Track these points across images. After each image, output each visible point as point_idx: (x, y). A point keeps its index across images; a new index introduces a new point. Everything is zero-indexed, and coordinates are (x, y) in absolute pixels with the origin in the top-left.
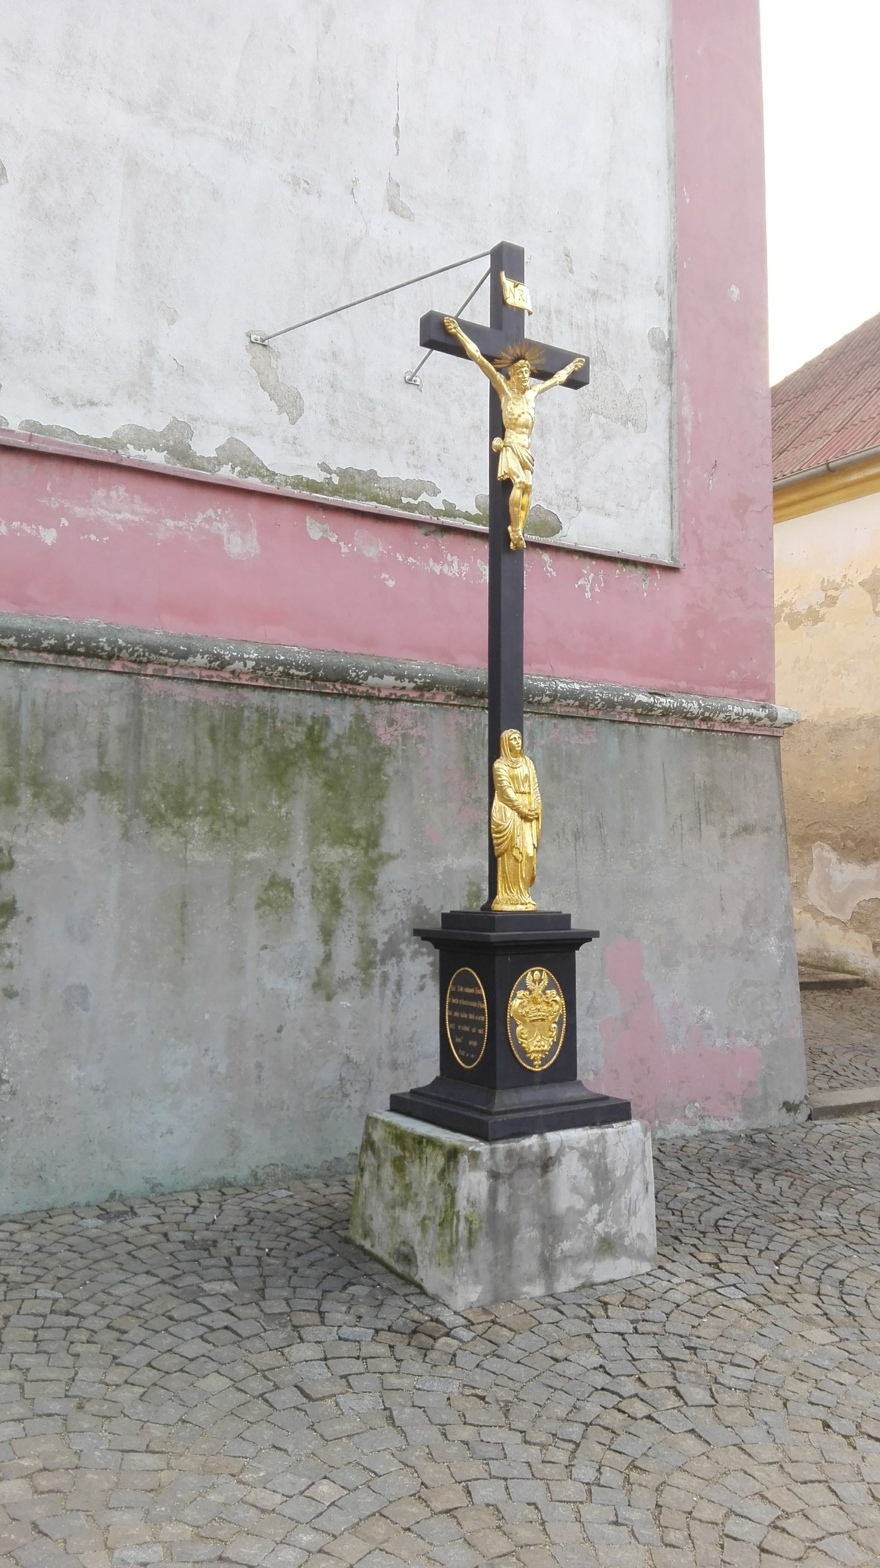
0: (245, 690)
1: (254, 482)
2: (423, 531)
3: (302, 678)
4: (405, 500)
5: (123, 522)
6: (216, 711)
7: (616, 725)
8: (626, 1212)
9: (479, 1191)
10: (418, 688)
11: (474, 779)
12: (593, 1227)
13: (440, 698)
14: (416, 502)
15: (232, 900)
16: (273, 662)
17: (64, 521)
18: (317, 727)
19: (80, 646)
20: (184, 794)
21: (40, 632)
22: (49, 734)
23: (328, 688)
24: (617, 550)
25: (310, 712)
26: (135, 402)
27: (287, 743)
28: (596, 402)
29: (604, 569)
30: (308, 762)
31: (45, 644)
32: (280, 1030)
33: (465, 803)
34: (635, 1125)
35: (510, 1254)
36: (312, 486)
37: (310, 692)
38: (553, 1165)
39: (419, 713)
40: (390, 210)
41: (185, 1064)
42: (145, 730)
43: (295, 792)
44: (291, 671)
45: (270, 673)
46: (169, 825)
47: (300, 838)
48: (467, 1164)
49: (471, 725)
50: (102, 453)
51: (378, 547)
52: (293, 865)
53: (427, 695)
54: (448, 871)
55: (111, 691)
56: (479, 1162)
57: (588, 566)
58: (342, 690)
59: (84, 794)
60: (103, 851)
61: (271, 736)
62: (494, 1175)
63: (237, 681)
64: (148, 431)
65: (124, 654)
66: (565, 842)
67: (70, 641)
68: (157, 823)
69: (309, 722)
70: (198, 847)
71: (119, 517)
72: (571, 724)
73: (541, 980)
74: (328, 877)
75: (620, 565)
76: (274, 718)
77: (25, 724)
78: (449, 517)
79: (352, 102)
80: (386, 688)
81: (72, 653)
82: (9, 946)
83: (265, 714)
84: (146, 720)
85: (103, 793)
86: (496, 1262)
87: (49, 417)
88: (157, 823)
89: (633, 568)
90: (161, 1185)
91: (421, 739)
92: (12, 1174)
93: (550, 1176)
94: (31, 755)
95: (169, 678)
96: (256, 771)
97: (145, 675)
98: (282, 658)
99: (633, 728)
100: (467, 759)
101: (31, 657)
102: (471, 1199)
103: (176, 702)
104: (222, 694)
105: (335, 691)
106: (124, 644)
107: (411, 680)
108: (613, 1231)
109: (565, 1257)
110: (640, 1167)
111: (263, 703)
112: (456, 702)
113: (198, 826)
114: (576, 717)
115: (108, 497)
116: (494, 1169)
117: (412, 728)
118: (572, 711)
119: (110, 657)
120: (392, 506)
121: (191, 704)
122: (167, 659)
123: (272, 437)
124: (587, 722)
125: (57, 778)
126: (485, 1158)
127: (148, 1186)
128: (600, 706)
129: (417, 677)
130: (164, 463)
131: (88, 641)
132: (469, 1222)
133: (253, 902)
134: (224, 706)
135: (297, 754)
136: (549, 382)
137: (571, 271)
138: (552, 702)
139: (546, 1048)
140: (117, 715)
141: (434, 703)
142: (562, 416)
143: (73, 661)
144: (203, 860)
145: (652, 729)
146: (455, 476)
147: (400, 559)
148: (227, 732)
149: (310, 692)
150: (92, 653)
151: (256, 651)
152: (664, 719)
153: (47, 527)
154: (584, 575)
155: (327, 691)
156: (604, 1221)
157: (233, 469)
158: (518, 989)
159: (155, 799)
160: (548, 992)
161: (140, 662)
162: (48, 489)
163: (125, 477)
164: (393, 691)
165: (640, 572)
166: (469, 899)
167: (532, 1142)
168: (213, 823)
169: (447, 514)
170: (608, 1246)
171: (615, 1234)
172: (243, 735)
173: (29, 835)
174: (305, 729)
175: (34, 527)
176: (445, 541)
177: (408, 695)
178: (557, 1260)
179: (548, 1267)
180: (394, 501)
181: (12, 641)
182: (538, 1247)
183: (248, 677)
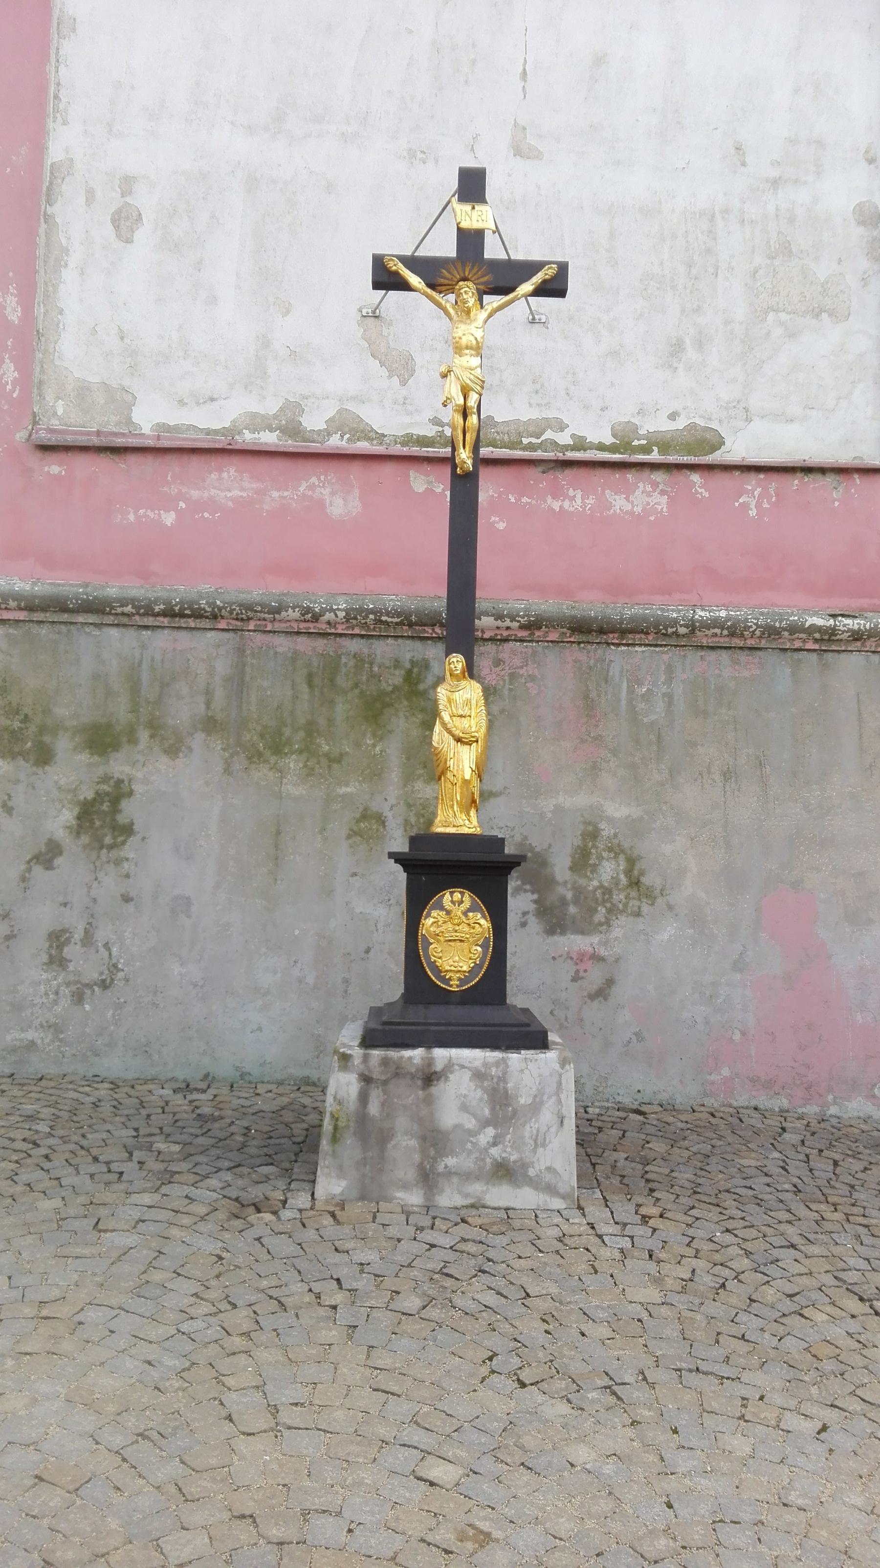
0: (344, 638)
1: (363, 446)
2: (540, 469)
3: (397, 624)
4: (525, 441)
5: (231, 499)
6: (314, 659)
7: (789, 654)
8: (532, 1143)
9: (348, 1091)
10: (522, 627)
11: (595, 716)
12: (486, 1150)
13: (554, 636)
14: (539, 441)
15: (323, 829)
16: (363, 611)
17: (182, 505)
18: (415, 670)
19: (185, 609)
20: (281, 734)
21: (150, 600)
22: (164, 685)
23: (427, 632)
24: (803, 458)
25: (408, 656)
26: (251, 392)
27: (384, 685)
28: (777, 299)
29: (774, 483)
30: (405, 703)
31: (157, 609)
32: (368, 951)
33: (583, 741)
34: (551, 1055)
35: (382, 1157)
36: (423, 441)
37: (408, 637)
38: (438, 1080)
39: (530, 651)
40: (515, 155)
41: (275, 972)
42: (247, 678)
43: (391, 732)
44: (384, 618)
45: (363, 621)
46: (266, 761)
47: (394, 775)
48: (337, 1065)
49: (592, 662)
50: (220, 441)
51: (488, 491)
52: (386, 799)
53: (537, 633)
54: (559, 810)
55: (219, 646)
56: (349, 1064)
57: (752, 482)
58: (442, 633)
59: (192, 734)
60: (207, 784)
61: (368, 680)
62: (366, 1079)
63: (333, 631)
64: (263, 416)
65: (223, 612)
66: (710, 782)
67: (176, 605)
68: (255, 759)
69: (408, 665)
70: (294, 782)
71: (229, 495)
72: (724, 655)
73: (461, 902)
74: (422, 812)
75: (799, 475)
76: (371, 664)
77: (145, 677)
78: (579, 450)
79: (474, 62)
80: (490, 629)
81: (182, 615)
82: (127, 859)
83: (362, 660)
84: (248, 669)
85: (209, 734)
86: (364, 1162)
87: (175, 417)
88: (255, 759)
89: (819, 477)
90: (250, 1074)
91: (532, 678)
92: (123, 1046)
93: (434, 1090)
94: (149, 703)
95: (270, 632)
96: (351, 713)
97: (249, 631)
98: (371, 606)
99: (814, 657)
100: (586, 697)
101: (150, 621)
102: (338, 1097)
103: (276, 653)
104: (320, 643)
105: (434, 635)
106: (222, 605)
107: (513, 619)
108: (513, 1158)
109: (449, 1173)
110: (554, 1099)
111: (361, 649)
112: (572, 640)
113: (293, 763)
114: (730, 648)
115: (220, 479)
116: (367, 1073)
117: (522, 667)
118: (724, 641)
119: (215, 617)
120: (511, 449)
121: (290, 655)
122: (263, 615)
123: (381, 401)
124: (747, 652)
125: (170, 721)
126: (357, 1061)
127: (238, 1074)
128: (758, 633)
129: (519, 616)
130: (277, 441)
131: (191, 603)
132: (335, 1119)
133: (344, 832)
134: (322, 655)
135: (394, 696)
136: (511, 296)
137: (744, 164)
138: (693, 632)
139: (465, 968)
140: (223, 667)
141: (548, 642)
142: (727, 322)
143: (185, 622)
144: (297, 793)
145: (843, 656)
146: (586, 407)
147: (513, 500)
148: (323, 679)
149: (408, 637)
150: (198, 614)
151: (346, 602)
152: (859, 644)
153: (167, 511)
154: (747, 492)
155: (426, 635)
156: (500, 1146)
157: (342, 437)
158: (433, 908)
159: (255, 738)
160: (471, 914)
161: (242, 620)
162: (169, 478)
163: (235, 460)
164: (498, 632)
165: (830, 479)
166: (584, 839)
167: (416, 1054)
168: (308, 760)
169: (574, 448)
170: (505, 1172)
171: (515, 1162)
172: (340, 681)
173: (145, 769)
174: (403, 672)
175: (156, 512)
176: (565, 477)
177: (516, 635)
178: (439, 1174)
179: (428, 1178)
180: (513, 443)
181: (129, 609)
182: (417, 1158)
183: (344, 627)
